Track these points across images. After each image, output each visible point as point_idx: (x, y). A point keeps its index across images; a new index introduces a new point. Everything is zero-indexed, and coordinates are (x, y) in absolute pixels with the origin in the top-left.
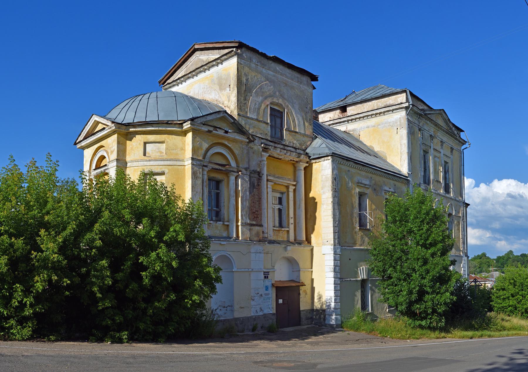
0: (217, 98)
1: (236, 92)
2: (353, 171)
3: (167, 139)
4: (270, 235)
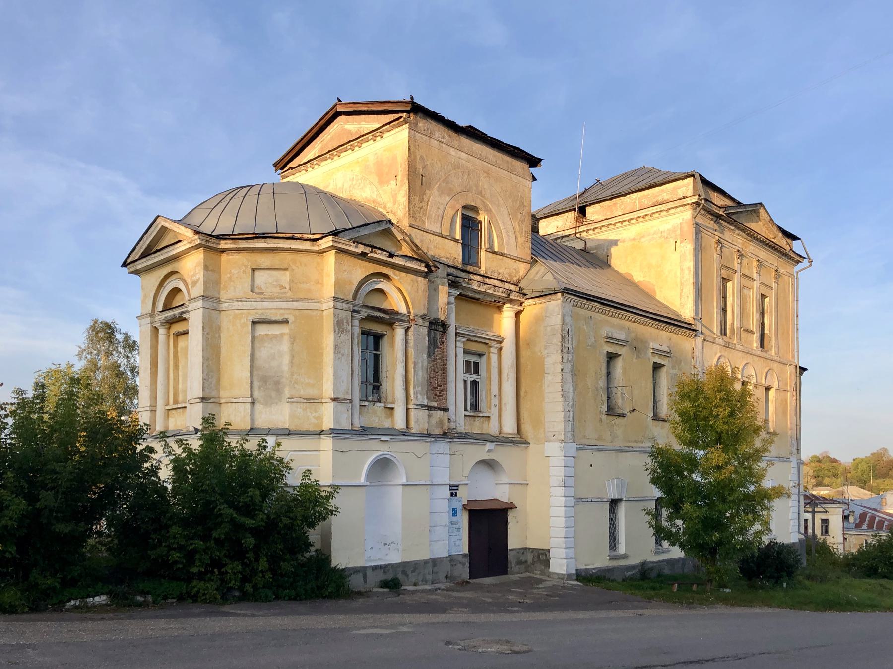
0: (374, 197)
1: (407, 187)
2: (600, 317)
3: (292, 265)
4: (459, 424)
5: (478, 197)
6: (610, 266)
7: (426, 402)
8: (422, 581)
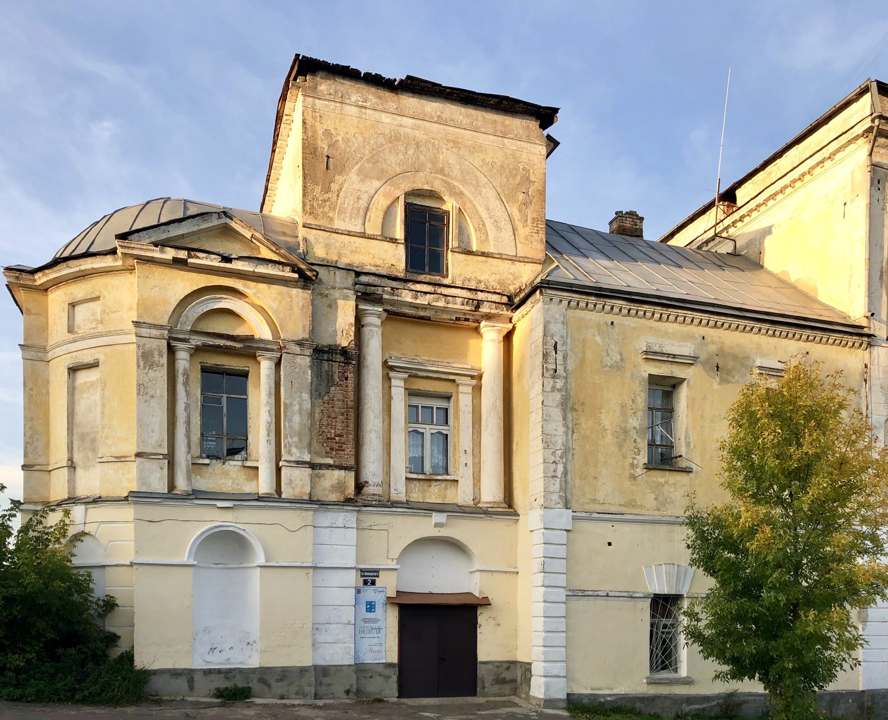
5: (436, 178)
6: (762, 267)
7: (307, 458)
8: (297, 693)
